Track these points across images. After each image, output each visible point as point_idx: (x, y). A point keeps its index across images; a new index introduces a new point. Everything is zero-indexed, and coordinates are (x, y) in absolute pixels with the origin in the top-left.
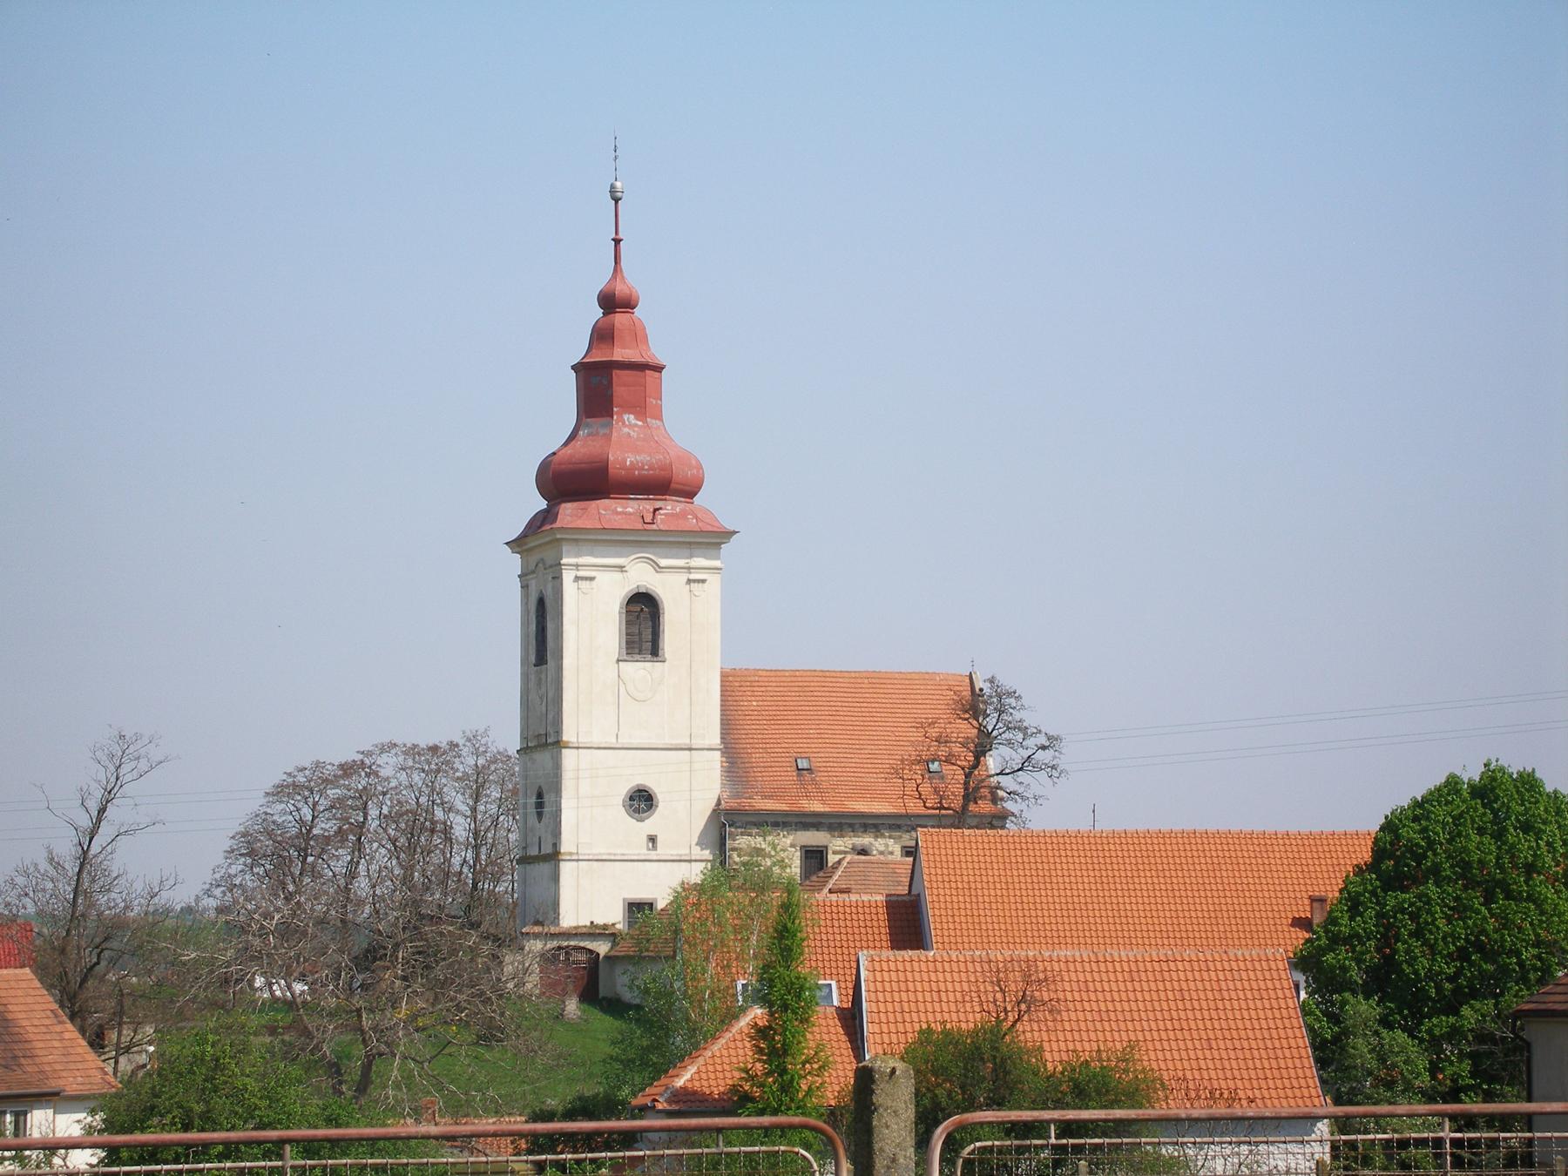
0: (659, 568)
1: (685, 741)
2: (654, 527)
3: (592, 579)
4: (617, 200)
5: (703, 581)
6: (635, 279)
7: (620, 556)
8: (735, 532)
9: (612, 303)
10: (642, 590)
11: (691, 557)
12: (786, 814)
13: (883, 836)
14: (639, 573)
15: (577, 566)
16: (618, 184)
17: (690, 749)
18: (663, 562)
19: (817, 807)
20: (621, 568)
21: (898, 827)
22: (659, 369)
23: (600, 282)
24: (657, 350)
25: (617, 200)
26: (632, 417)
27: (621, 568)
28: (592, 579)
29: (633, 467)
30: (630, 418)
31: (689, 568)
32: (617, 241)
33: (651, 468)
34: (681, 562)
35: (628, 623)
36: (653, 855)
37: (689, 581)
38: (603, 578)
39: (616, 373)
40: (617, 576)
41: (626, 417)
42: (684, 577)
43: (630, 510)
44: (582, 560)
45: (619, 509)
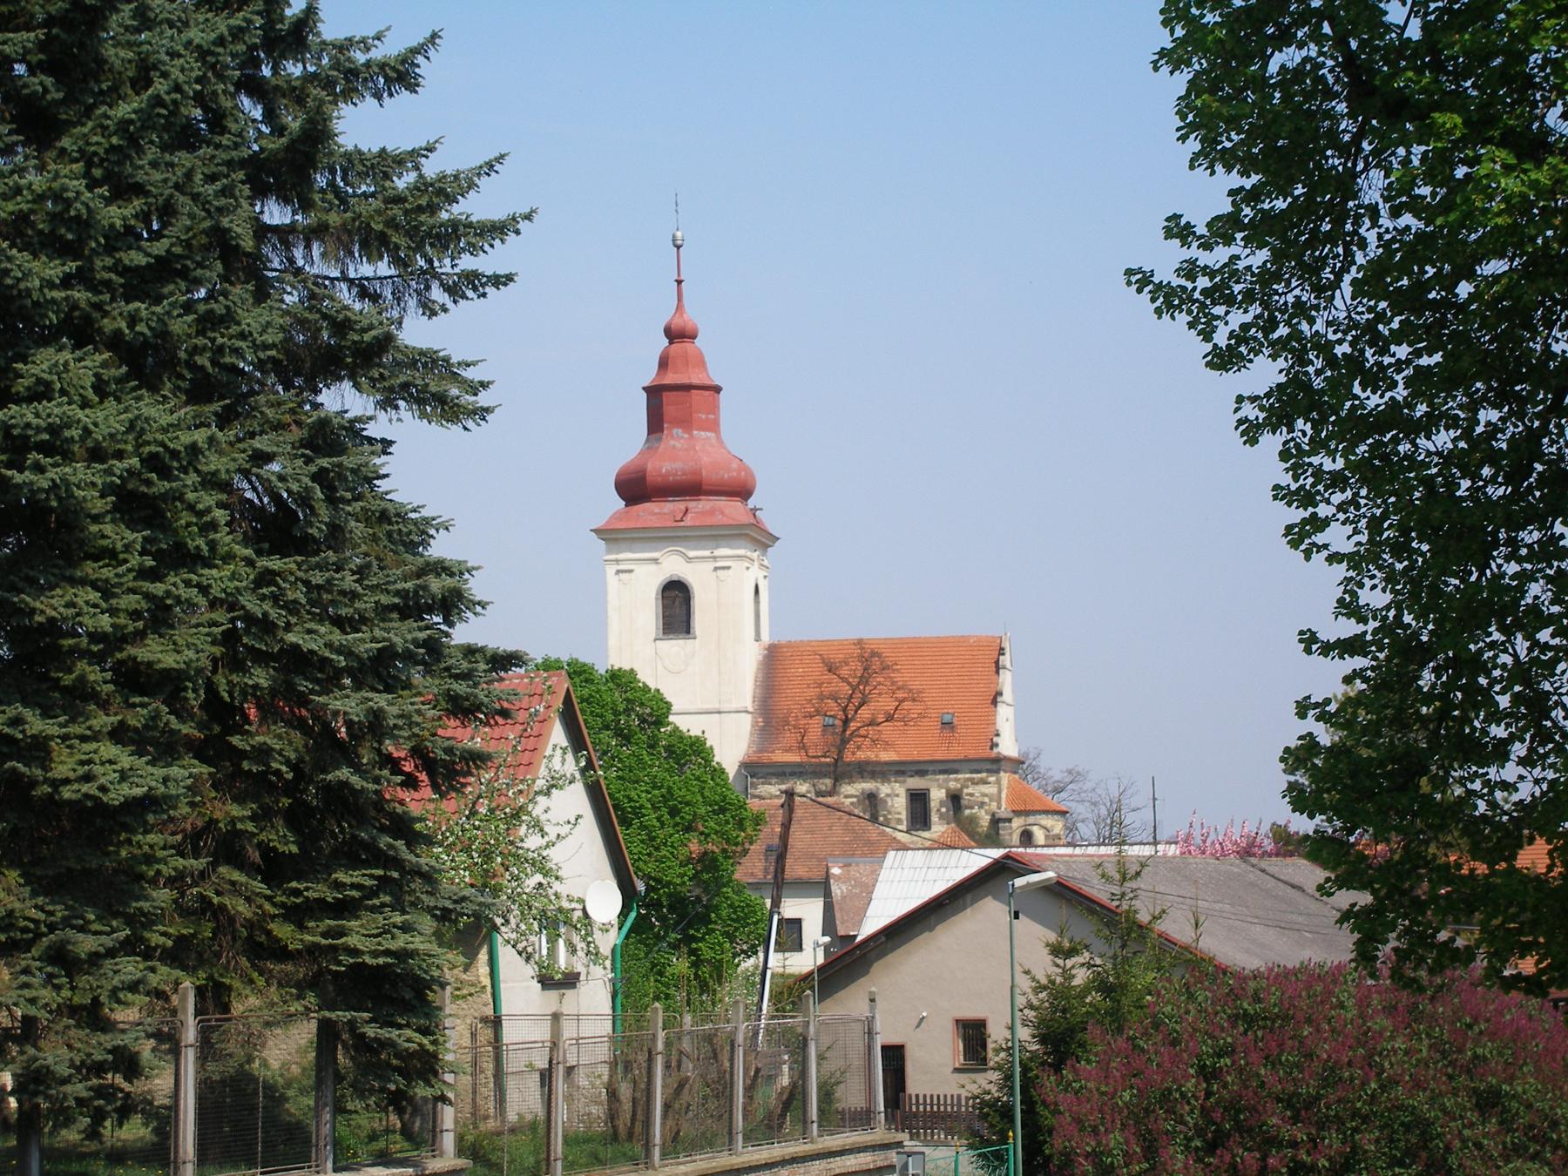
0: (689, 560)
1: (716, 706)
2: (682, 524)
3: (631, 571)
4: (678, 247)
5: (729, 568)
6: (694, 315)
7: (656, 550)
8: (595, 531)
9: (677, 334)
10: (675, 579)
11: (717, 548)
12: (800, 765)
13: (889, 781)
14: (673, 564)
15: (617, 561)
16: (679, 234)
17: (719, 712)
18: (692, 554)
19: (886, 756)
20: (656, 561)
21: (903, 773)
22: (717, 389)
23: (665, 314)
24: (716, 376)
25: (678, 247)
26: (680, 431)
27: (656, 561)
28: (631, 571)
29: (668, 474)
30: (678, 432)
31: (715, 558)
32: (679, 282)
33: (684, 474)
34: (707, 553)
35: (664, 607)
36: (916, 783)
37: (716, 569)
38: (642, 571)
39: (665, 394)
40: (653, 567)
41: (675, 431)
42: (713, 565)
43: (666, 511)
44: (718, 552)
45: (656, 511)
